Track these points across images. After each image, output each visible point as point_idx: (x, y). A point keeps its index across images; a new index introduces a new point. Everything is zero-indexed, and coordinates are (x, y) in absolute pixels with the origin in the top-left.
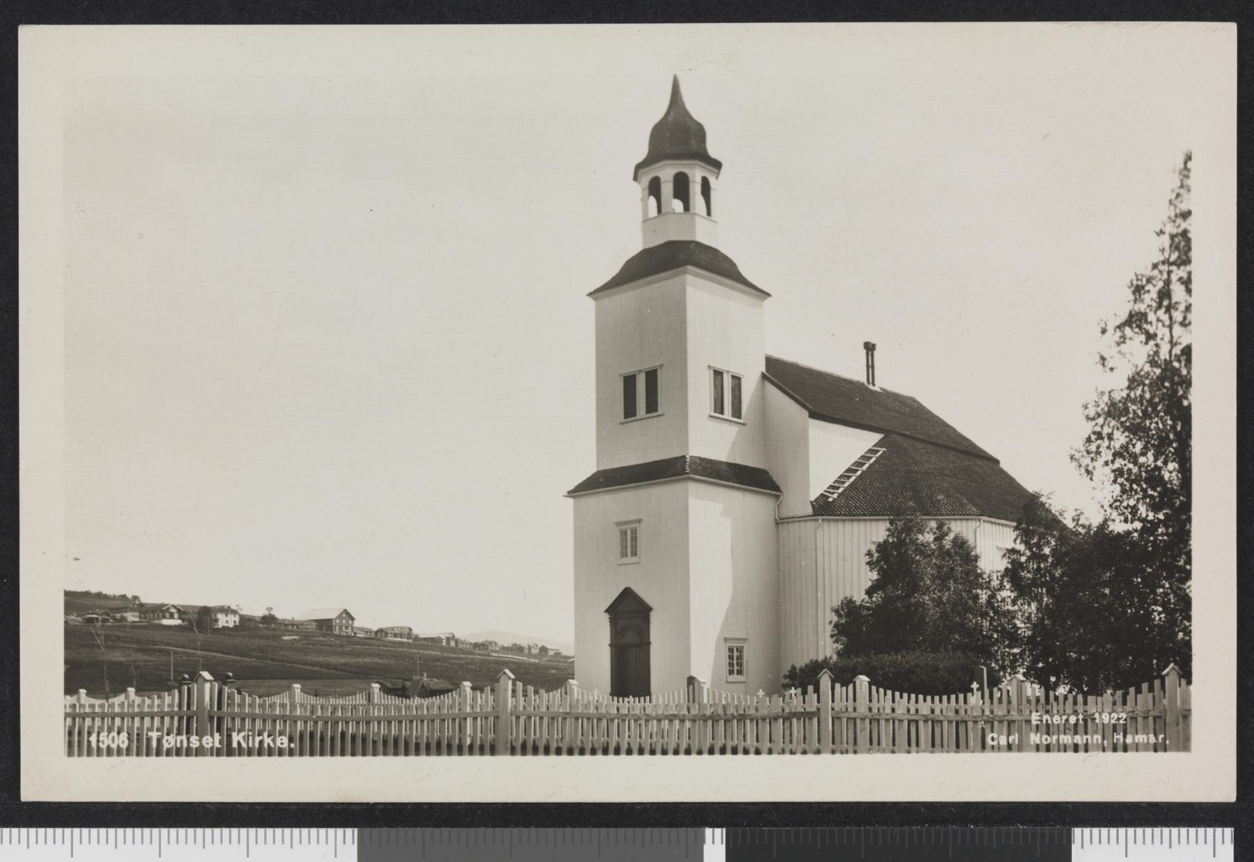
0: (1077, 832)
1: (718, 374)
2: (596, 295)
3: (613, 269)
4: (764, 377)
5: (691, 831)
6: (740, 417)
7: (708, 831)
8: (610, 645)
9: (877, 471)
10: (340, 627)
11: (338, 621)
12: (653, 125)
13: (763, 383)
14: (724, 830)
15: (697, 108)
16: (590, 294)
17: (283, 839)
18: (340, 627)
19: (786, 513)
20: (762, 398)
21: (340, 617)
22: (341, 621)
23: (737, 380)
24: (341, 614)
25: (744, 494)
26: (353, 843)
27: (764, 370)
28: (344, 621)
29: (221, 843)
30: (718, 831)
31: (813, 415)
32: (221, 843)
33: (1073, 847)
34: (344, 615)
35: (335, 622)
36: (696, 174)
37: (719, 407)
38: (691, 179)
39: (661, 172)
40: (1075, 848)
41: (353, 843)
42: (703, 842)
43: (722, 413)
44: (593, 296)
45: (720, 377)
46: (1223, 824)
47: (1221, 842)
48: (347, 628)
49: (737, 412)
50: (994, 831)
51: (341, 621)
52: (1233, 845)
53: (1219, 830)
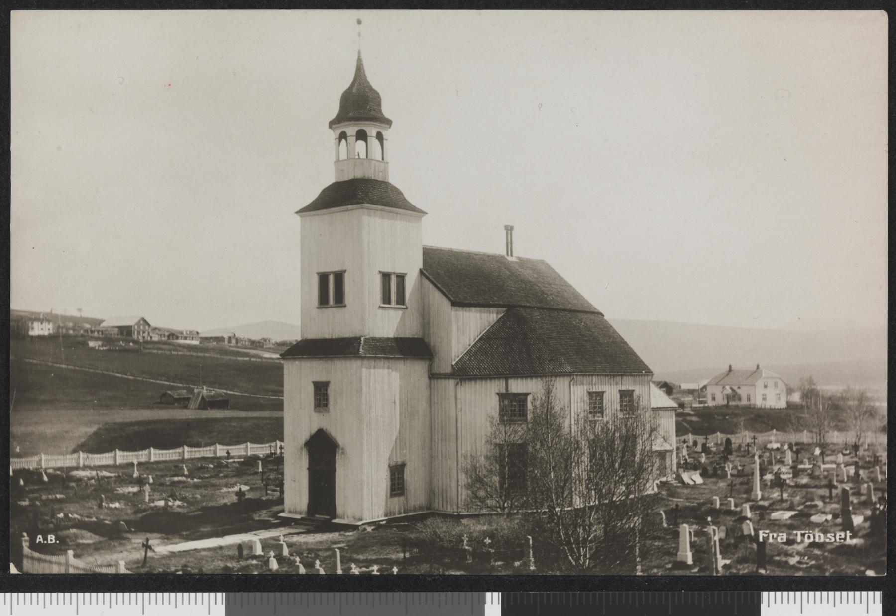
0: (765, 594)
1: (386, 276)
2: (303, 214)
3: (313, 195)
4: (421, 272)
5: (476, 594)
6: (403, 303)
7: (488, 594)
8: (308, 469)
9: (502, 338)
10: (139, 333)
11: (136, 327)
12: (342, 92)
13: (421, 277)
14: (500, 593)
15: (375, 80)
16: (297, 213)
17: (90, 601)
18: (139, 333)
19: (436, 370)
20: (420, 287)
21: (138, 324)
22: (139, 327)
23: (401, 277)
24: (140, 321)
25: (463, 309)
26: (222, 604)
27: (421, 266)
28: (142, 328)
29: (123, 604)
30: (495, 594)
31: (454, 304)
32: (123, 604)
33: (762, 605)
34: (142, 322)
35: (134, 328)
36: (372, 131)
37: (386, 299)
38: (368, 134)
39: (349, 129)
40: (763, 607)
41: (222, 604)
42: (484, 602)
43: (389, 303)
44: (300, 214)
45: (387, 279)
46: (874, 589)
47: (69, 603)
48: (144, 332)
49: (401, 299)
50: (631, 595)
51: (139, 327)
52: (881, 605)
53: (871, 593)
